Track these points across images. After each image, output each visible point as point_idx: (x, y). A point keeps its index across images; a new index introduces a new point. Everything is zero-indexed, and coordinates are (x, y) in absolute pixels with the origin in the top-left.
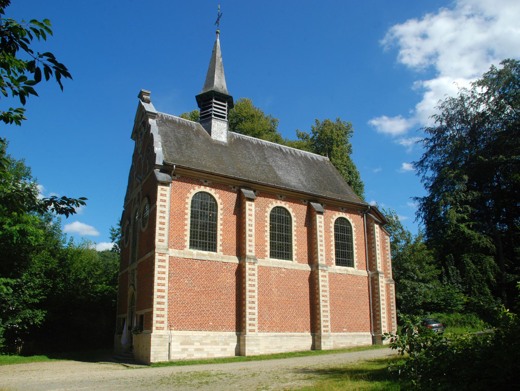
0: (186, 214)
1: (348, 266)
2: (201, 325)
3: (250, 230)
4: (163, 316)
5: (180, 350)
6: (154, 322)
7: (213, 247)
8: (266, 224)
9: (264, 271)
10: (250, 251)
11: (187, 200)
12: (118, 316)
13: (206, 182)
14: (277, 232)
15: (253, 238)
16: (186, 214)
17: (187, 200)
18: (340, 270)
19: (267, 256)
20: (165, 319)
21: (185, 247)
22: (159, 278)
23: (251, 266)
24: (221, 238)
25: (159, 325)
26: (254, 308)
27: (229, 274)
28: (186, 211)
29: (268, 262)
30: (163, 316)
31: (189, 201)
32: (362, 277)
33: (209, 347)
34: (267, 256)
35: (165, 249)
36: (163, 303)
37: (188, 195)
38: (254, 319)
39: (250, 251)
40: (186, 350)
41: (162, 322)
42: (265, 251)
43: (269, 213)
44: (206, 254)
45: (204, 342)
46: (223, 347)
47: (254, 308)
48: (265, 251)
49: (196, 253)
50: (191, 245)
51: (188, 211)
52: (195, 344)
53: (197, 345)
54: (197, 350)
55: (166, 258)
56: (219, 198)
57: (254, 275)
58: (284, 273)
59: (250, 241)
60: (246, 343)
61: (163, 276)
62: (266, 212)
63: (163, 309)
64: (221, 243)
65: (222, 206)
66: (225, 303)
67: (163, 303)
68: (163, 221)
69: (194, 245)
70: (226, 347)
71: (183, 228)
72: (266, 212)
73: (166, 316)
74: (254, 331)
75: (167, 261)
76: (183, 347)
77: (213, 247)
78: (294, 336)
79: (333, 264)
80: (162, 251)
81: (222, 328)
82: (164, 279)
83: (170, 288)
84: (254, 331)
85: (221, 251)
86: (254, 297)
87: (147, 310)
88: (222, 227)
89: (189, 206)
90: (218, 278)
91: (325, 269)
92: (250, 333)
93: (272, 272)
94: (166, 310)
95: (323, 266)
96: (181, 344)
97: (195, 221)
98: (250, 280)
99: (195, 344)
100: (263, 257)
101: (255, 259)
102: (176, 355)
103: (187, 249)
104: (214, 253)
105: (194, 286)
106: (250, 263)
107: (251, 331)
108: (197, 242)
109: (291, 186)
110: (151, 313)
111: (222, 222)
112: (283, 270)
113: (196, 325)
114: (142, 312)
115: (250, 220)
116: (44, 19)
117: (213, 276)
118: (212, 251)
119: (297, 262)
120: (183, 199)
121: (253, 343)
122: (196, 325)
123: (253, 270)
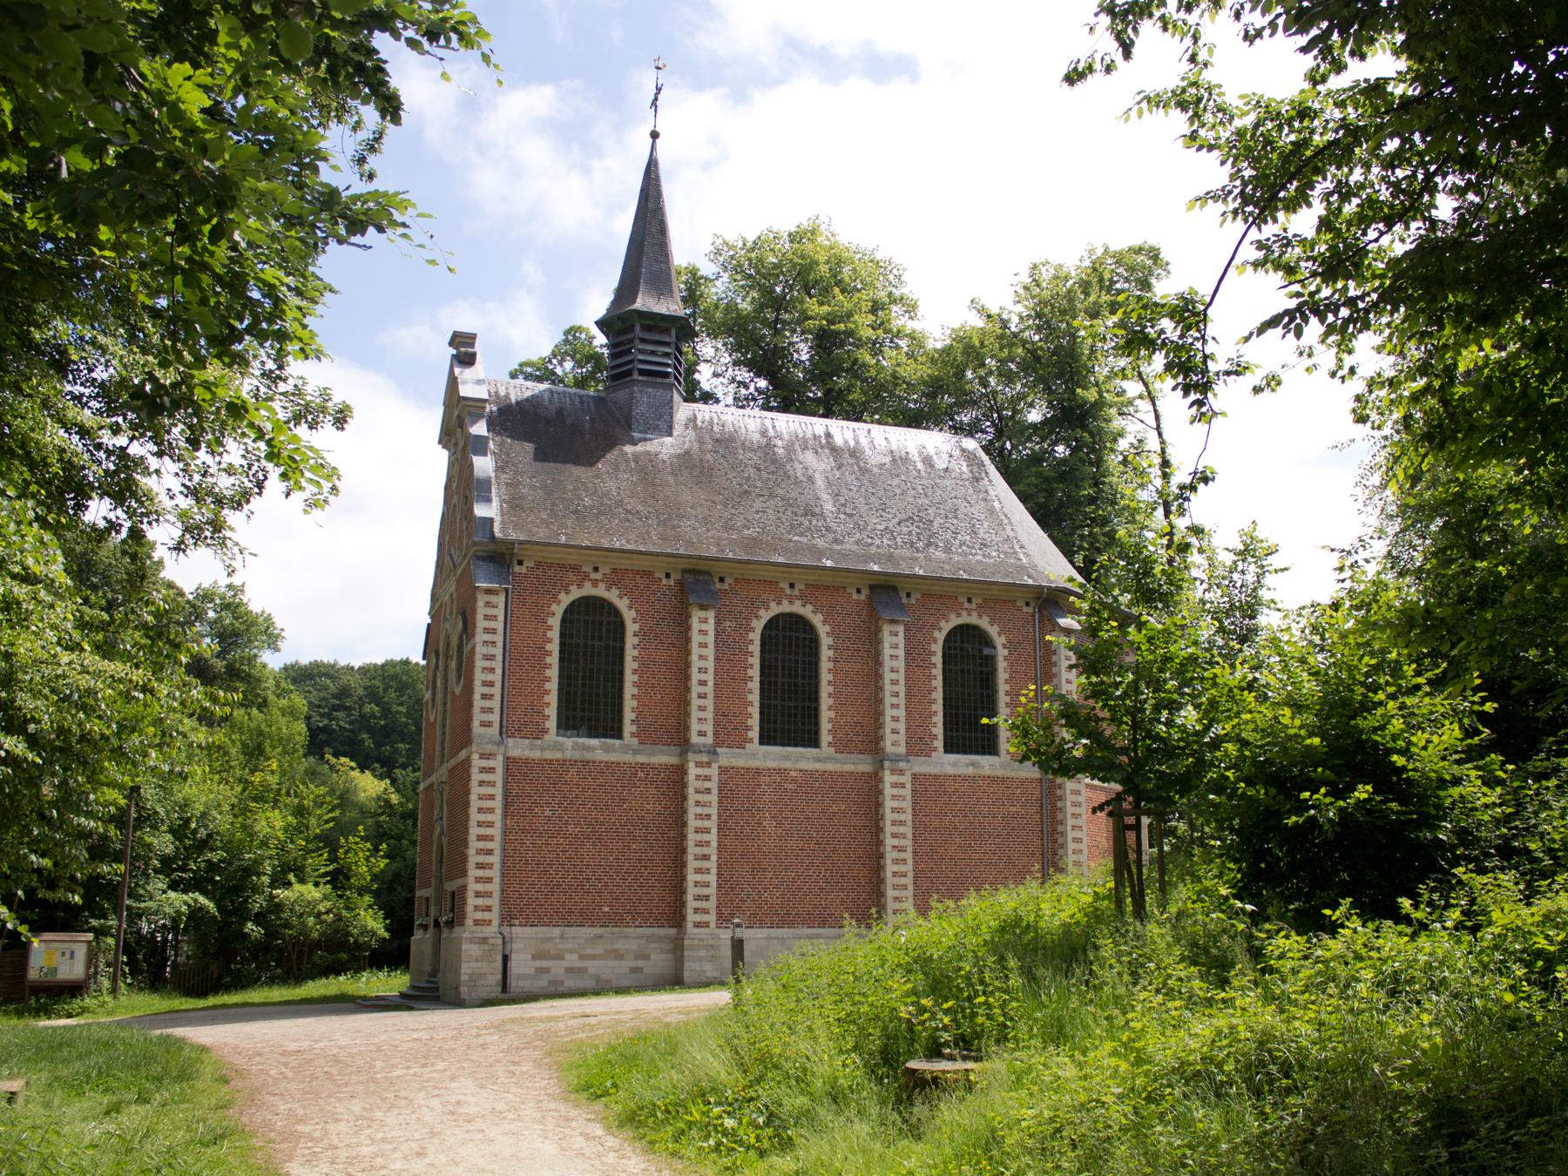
0: (549, 654)
1: (983, 753)
2: (582, 913)
3: (703, 683)
4: (489, 895)
5: (532, 971)
6: (469, 909)
7: (612, 729)
8: (751, 660)
9: (925, 787)
10: (702, 734)
11: (550, 621)
12: (418, 893)
13: (596, 569)
14: (800, 681)
15: (709, 702)
16: (549, 654)
17: (550, 621)
18: (955, 764)
19: (935, 749)
20: (495, 902)
21: (546, 731)
22: (480, 810)
23: (700, 771)
24: (635, 703)
25: (479, 915)
26: (708, 871)
27: (652, 791)
28: (549, 647)
29: (754, 756)
30: (489, 895)
31: (555, 622)
32: (1032, 781)
33: (602, 963)
34: (751, 741)
35: (494, 743)
36: (490, 866)
37: (554, 607)
38: (707, 898)
39: (702, 734)
40: (547, 970)
41: (488, 909)
42: (748, 728)
43: (759, 632)
44: (597, 749)
45: (589, 951)
46: (633, 964)
47: (708, 871)
48: (748, 728)
49: (573, 746)
50: (559, 726)
51: (554, 647)
52: (568, 956)
53: (572, 960)
54: (569, 970)
55: (498, 763)
56: (630, 608)
57: (708, 791)
58: (794, 780)
59: (702, 709)
60: (686, 953)
61: (490, 804)
62: (752, 630)
63: (489, 880)
64: (633, 716)
65: (636, 627)
66: (640, 861)
67: (490, 866)
68: (490, 677)
69: (769, 738)
70: (640, 963)
71: (540, 687)
72: (752, 630)
73: (497, 895)
74: (707, 925)
75: (500, 770)
76: (538, 964)
77: (612, 729)
78: (818, 936)
79: (935, 749)
80: (489, 748)
81: (633, 918)
82: (491, 811)
83: (506, 831)
84: (707, 925)
85: (633, 735)
86: (708, 843)
87: (460, 882)
88: (635, 678)
89: (555, 634)
90: (624, 800)
91: (902, 765)
92: (696, 930)
93: (762, 779)
94: (497, 880)
95: (896, 759)
96: (534, 957)
97: (769, 683)
98: (698, 803)
99: (568, 956)
100: (742, 743)
101: (712, 752)
102: (521, 983)
103: (755, 746)
104: (617, 742)
105: (567, 823)
106: (699, 764)
107: (698, 925)
108: (796, 731)
109: (1049, 581)
110: (464, 888)
111: (635, 665)
112: (793, 774)
113: (570, 913)
114: (450, 886)
115: (701, 657)
116: (431, 267)
117: (613, 798)
118: (612, 737)
119: (832, 750)
120: (541, 618)
121: (702, 953)
122: (570, 913)
123: (707, 778)
